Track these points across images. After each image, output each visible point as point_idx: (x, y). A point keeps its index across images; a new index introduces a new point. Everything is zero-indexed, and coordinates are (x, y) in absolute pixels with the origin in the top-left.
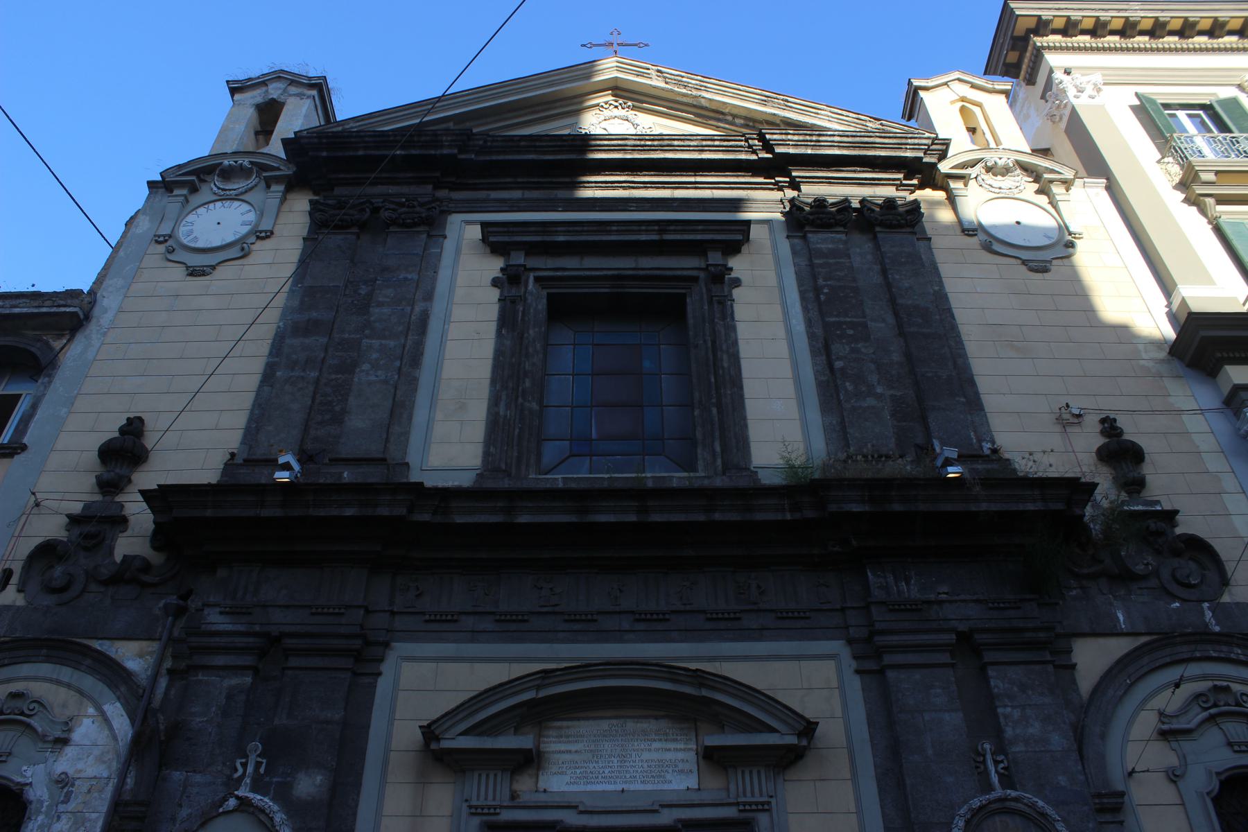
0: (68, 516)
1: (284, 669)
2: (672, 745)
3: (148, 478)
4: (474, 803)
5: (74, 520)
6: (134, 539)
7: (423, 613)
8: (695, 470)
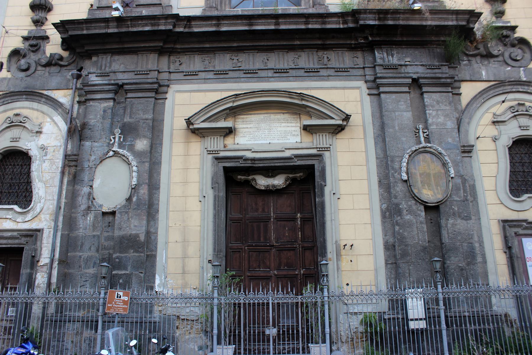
0: (22, 37)
1: (126, 98)
2: (290, 125)
3: (54, 17)
4: (209, 149)
5: (26, 39)
6: (54, 46)
7: (183, 72)
8: (300, 5)
